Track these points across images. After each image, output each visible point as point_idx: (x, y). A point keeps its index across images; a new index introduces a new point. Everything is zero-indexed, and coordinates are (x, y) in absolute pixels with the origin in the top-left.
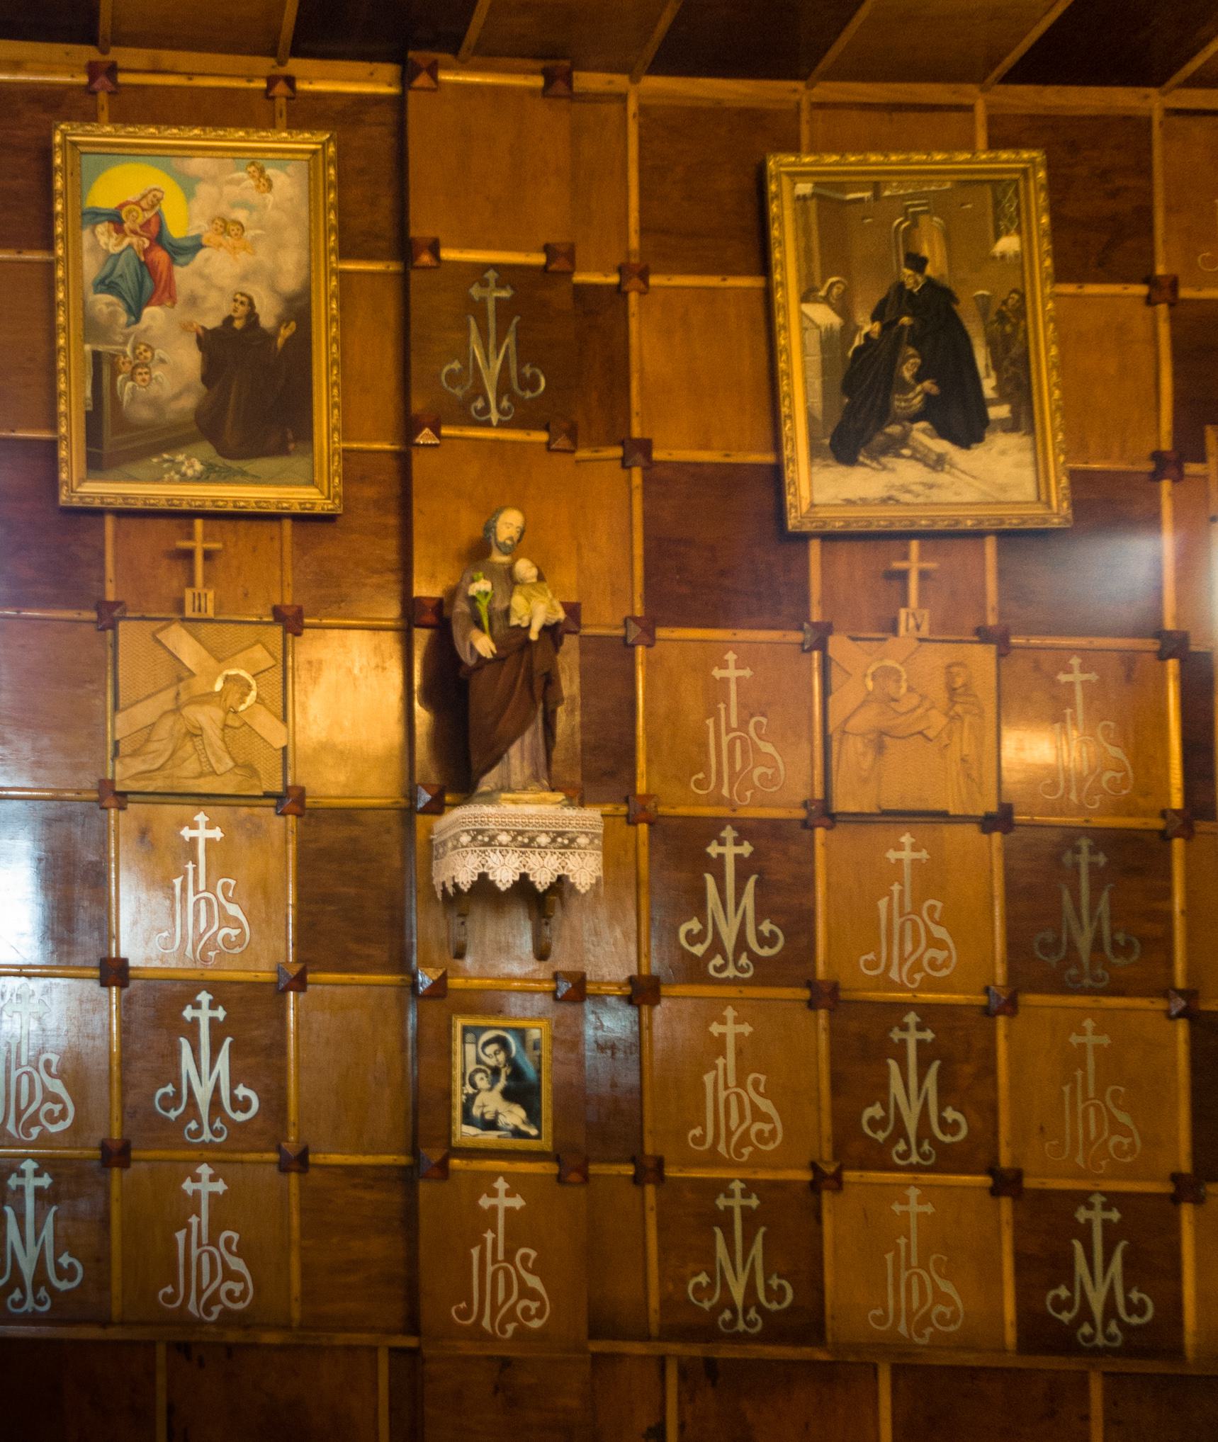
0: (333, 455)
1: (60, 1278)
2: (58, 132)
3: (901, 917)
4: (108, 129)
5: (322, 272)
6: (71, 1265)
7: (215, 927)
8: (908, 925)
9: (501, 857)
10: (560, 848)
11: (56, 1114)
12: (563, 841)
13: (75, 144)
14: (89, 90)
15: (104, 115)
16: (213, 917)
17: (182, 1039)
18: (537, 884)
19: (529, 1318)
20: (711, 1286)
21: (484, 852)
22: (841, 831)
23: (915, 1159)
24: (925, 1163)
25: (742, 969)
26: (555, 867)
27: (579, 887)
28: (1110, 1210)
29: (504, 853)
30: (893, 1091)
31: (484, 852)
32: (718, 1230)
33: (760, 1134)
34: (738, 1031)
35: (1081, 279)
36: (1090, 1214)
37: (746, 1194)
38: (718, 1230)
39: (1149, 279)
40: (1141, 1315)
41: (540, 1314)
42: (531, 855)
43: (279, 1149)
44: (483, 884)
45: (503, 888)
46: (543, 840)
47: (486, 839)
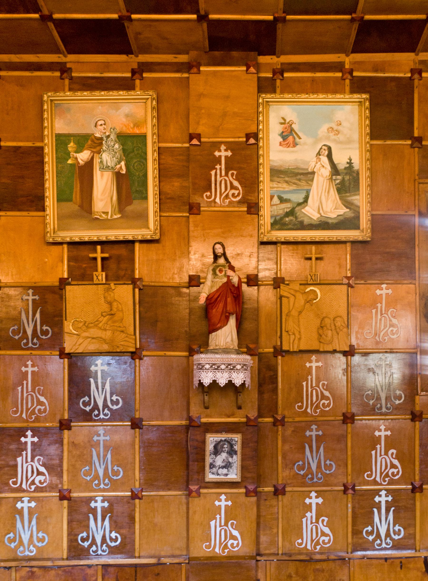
0: (368, 221)
1: (38, 542)
2: (261, 98)
3: (27, 393)
4: (68, 93)
5: (364, 151)
6: (43, 536)
7: (35, 405)
8: (29, 397)
9: (206, 374)
10: (214, 370)
11: (395, 473)
12: (231, 368)
13: (267, 102)
14: (132, 79)
15: (137, 88)
16: (34, 402)
17: (93, 449)
18: (219, 383)
19: (233, 547)
20: (15, 537)
21: (215, 372)
22: (287, 358)
23: (102, 486)
24: (106, 487)
25: (106, 415)
26: (211, 377)
27: (204, 384)
28: (104, 502)
29: (238, 373)
30: (94, 459)
31: (215, 372)
32: (17, 516)
33: (393, 473)
34: (32, 440)
35: (384, 138)
36: (380, 499)
37: (103, 501)
38: (17, 516)
39: (412, 138)
40: (399, 535)
41: (238, 545)
42: (218, 373)
43: (412, 484)
44: (230, 384)
45: (222, 386)
46: (223, 367)
47: (216, 367)
